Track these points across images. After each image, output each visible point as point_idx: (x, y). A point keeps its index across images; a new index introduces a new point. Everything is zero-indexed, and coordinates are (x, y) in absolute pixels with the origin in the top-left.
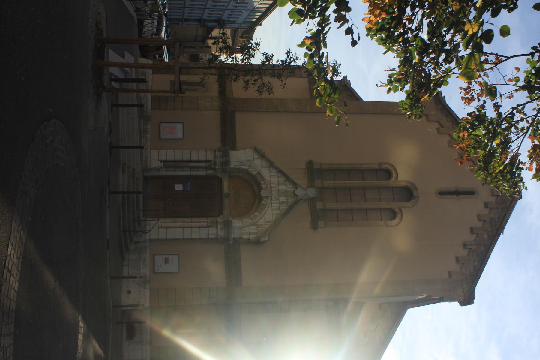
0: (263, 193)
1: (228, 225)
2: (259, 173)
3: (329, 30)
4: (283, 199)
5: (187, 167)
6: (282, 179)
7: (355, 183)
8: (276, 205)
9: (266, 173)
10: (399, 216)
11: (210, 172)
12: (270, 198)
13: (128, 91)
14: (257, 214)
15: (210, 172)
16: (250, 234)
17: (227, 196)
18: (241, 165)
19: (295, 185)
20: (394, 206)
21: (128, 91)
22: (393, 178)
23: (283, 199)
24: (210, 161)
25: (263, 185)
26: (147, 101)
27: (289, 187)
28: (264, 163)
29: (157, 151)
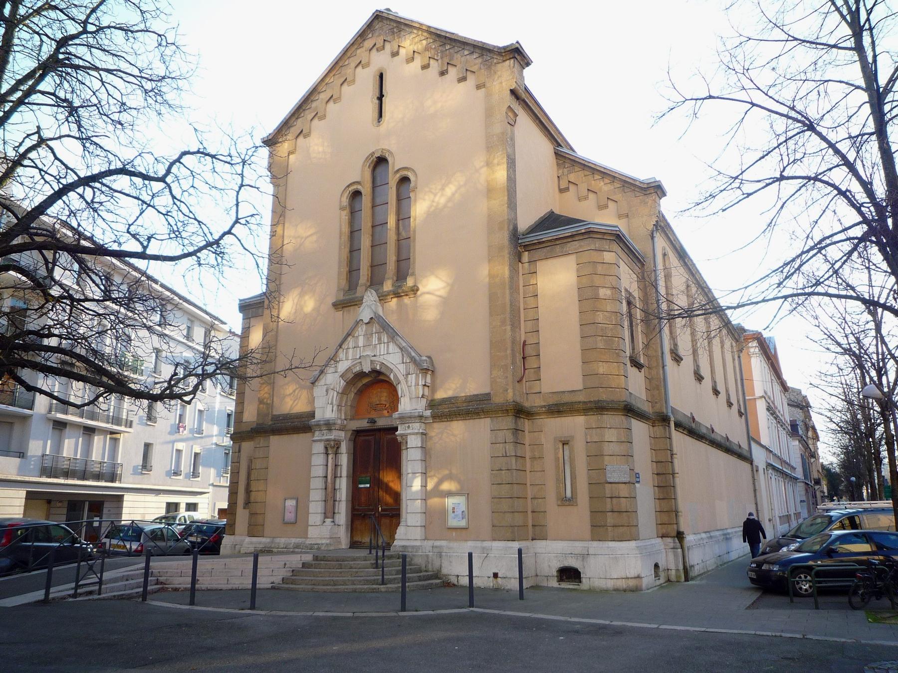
0: (367, 369)
1: (406, 419)
2: (342, 376)
3: (415, 351)
4: (375, 340)
5: (334, 483)
6: (351, 342)
7: (365, 242)
8: (382, 349)
9: (343, 366)
10: (410, 175)
11: (344, 448)
12: (374, 358)
13: (368, 582)
14: (392, 377)
15: (344, 448)
16: (417, 384)
17: (373, 421)
18: (332, 404)
19: (358, 323)
20: (393, 181)
21: (368, 582)
22: (359, 187)
23: (375, 340)
24: (326, 448)
25: (358, 369)
26: (260, 543)
27: (361, 331)
28: (330, 370)
29: (310, 528)
